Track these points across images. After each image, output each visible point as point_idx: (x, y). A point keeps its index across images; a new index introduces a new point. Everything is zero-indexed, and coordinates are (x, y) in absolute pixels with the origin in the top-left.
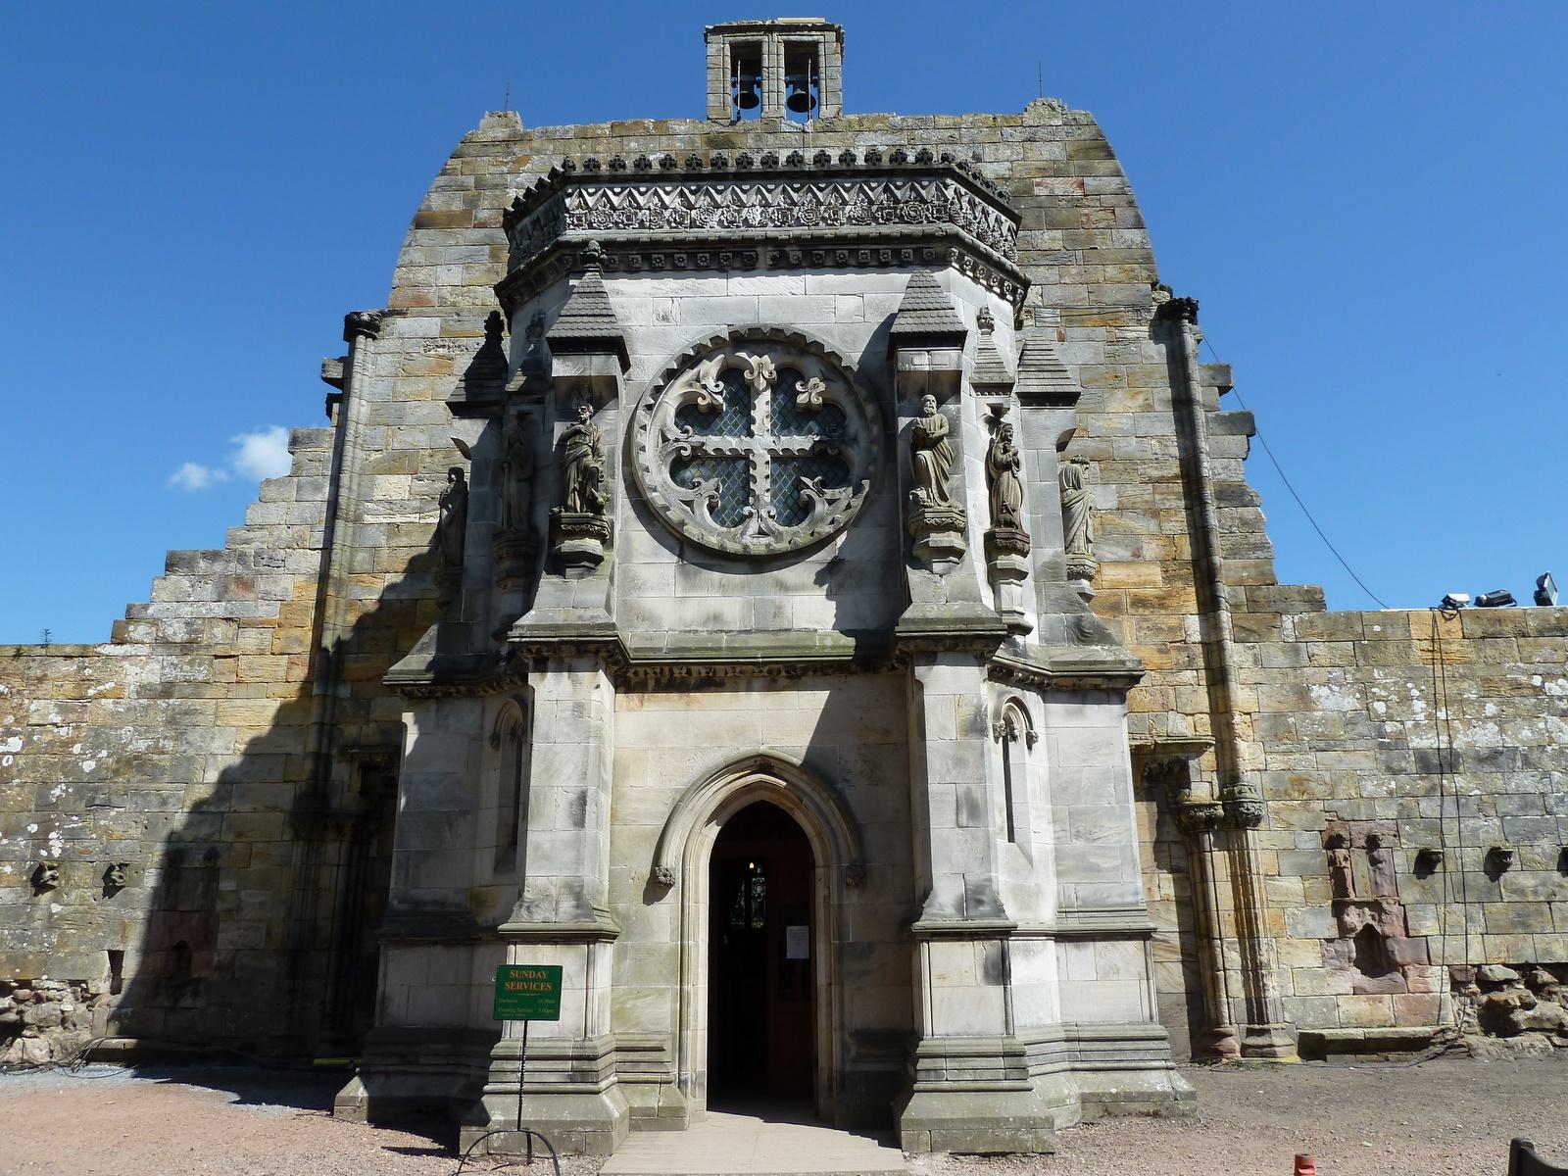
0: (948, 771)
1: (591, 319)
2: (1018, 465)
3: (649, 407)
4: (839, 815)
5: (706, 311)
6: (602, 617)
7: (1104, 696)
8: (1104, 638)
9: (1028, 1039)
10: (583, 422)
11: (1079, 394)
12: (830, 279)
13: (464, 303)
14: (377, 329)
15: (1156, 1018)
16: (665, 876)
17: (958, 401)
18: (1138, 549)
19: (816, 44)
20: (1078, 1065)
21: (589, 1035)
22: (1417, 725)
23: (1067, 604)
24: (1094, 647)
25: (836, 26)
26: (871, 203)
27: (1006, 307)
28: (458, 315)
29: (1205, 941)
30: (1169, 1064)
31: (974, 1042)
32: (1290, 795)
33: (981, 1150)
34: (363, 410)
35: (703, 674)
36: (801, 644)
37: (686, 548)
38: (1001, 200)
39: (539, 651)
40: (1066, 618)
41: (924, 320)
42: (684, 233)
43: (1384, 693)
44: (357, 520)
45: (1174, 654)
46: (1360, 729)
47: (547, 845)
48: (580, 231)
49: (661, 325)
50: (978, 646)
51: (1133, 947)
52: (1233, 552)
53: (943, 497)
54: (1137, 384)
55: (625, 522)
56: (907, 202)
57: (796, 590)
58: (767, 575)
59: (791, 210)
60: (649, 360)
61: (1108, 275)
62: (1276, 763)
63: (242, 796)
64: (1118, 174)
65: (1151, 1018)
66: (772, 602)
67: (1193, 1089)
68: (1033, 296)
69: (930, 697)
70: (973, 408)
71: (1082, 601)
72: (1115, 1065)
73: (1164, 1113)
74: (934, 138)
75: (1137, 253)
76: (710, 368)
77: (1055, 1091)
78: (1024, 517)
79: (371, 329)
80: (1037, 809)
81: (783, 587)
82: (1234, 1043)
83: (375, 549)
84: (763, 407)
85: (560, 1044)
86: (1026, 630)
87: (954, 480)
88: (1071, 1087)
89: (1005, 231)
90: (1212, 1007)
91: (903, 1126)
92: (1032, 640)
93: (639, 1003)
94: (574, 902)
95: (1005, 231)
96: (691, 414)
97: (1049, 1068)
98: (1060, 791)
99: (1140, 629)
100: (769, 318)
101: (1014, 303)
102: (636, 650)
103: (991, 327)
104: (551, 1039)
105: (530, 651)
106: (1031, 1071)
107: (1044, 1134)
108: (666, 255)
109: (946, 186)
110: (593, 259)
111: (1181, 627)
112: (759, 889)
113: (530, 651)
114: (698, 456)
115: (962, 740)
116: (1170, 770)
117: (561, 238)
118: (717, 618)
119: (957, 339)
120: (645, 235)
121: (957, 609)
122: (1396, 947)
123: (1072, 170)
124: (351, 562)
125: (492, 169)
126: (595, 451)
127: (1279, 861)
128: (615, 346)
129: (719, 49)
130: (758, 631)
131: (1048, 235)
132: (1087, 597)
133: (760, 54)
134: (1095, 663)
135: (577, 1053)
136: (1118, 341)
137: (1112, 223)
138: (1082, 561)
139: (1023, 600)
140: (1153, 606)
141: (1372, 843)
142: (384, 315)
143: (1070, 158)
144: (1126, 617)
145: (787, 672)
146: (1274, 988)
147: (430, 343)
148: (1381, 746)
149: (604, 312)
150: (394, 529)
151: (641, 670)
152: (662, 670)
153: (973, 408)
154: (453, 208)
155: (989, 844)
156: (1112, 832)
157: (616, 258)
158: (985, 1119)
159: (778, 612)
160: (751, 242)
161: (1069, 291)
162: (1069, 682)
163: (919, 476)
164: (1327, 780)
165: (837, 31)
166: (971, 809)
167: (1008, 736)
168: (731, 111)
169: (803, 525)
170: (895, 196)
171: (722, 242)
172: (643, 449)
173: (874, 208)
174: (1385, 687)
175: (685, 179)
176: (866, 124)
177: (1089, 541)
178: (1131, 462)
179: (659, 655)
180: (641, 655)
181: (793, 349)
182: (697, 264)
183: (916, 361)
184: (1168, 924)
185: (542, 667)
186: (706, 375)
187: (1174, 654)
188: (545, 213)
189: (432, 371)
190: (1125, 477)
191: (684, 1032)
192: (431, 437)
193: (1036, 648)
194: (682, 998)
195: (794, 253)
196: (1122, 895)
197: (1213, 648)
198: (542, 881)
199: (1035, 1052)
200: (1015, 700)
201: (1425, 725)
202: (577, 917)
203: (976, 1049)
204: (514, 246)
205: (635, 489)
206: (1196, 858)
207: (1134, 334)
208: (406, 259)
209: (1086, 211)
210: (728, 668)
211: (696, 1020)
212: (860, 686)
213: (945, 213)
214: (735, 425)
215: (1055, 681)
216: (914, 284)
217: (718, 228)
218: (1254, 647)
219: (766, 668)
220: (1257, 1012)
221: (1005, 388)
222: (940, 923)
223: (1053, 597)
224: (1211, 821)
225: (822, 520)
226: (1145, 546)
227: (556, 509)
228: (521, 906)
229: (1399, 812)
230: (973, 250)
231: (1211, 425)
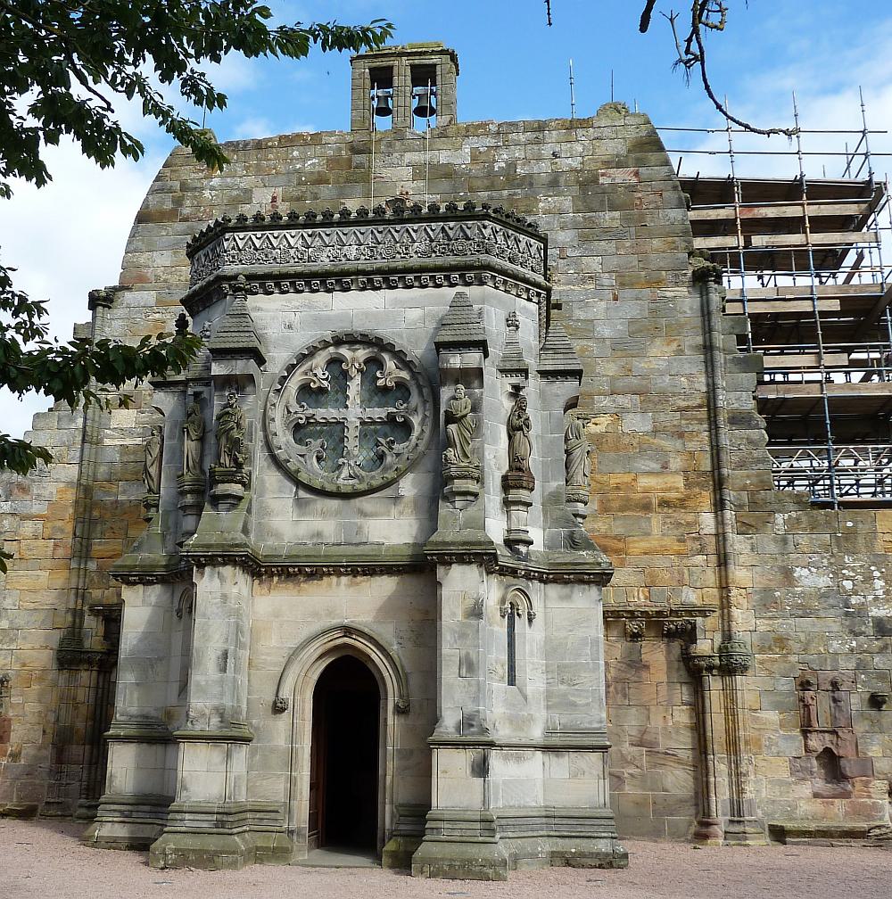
0: (455, 641)
3: (279, 391)
5: (318, 321)
12: (400, 293)
13: (173, 280)
14: (112, 301)
15: (608, 805)
16: (281, 703)
19: (435, 65)
20: (552, 833)
22: (876, 598)
24: (581, 553)
32: (772, 650)
40: (563, 531)
43: (852, 574)
44: (99, 442)
45: (689, 543)
46: (831, 601)
48: (233, 266)
49: (287, 332)
51: (595, 757)
52: (741, 465)
56: (457, 239)
57: (376, 516)
61: (655, 247)
62: (763, 625)
63: (24, 638)
65: (605, 804)
66: (356, 524)
69: (446, 592)
72: (578, 834)
76: (321, 359)
80: (533, 664)
81: (363, 514)
82: (719, 830)
84: (354, 386)
85: (210, 805)
96: (308, 393)
98: (551, 649)
100: (360, 327)
111: (696, 523)
118: (319, 534)
122: (848, 765)
123: (630, 163)
126: (238, 425)
127: (757, 700)
131: (608, 215)
140: (676, 507)
141: (835, 685)
143: (629, 151)
144: (654, 514)
146: (750, 792)
148: (847, 614)
149: (246, 329)
156: (585, 680)
159: (359, 530)
164: (803, 639)
170: (448, 235)
172: (273, 420)
174: (853, 569)
178: (664, 397)
180: (268, 559)
187: (689, 543)
194: (292, 781)
196: (590, 723)
197: (721, 537)
198: (200, 705)
201: (882, 599)
202: (221, 727)
205: (268, 446)
207: (672, 294)
212: (412, 583)
216: (454, 304)
218: (751, 538)
220: (737, 809)
222: (445, 738)
223: (555, 517)
224: (710, 668)
229: (858, 664)
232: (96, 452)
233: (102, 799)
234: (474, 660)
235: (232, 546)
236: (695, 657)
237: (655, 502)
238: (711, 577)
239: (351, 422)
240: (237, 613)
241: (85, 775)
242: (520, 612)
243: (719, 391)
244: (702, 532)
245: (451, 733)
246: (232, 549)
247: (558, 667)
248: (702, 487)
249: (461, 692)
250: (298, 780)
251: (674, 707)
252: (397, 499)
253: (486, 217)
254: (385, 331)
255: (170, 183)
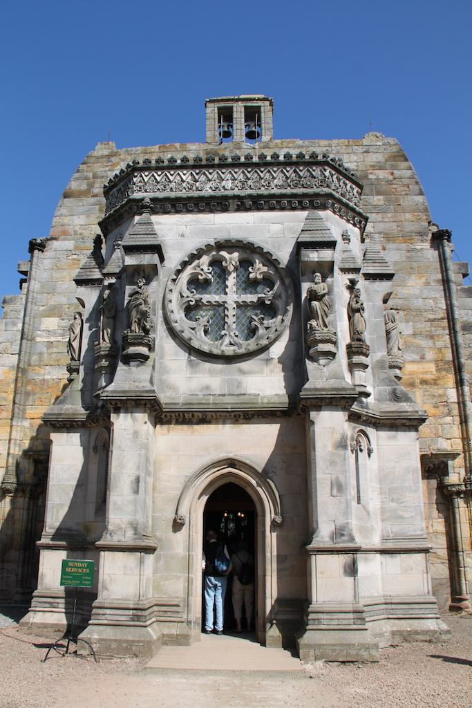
0: (327, 468)
1: (145, 236)
2: (363, 310)
4: (275, 553)
6: (149, 387)
7: (407, 428)
8: (407, 399)
9: (365, 604)
10: (140, 288)
11: (394, 274)
13: (86, 233)
14: (44, 247)
15: (431, 593)
16: (180, 519)
17: (333, 277)
18: (423, 355)
19: (260, 107)
20: (391, 616)
21: (141, 598)
23: (390, 382)
24: (402, 404)
25: (270, 98)
26: (287, 178)
27: (357, 230)
28: (83, 239)
29: (455, 553)
30: (438, 616)
31: (338, 606)
33: (341, 660)
34: (36, 286)
35: (201, 417)
36: (251, 401)
37: (192, 351)
38: (353, 177)
39: (116, 404)
40: (388, 389)
41: (315, 236)
42: (191, 194)
44: (33, 339)
47: (119, 503)
50: (343, 402)
51: (420, 556)
53: (326, 326)
54: (422, 272)
55: (161, 338)
58: (234, 365)
59: (247, 182)
60: (174, 258)
61: (407, 218)
64: (410, 169)
65: (428, 592)
66: (237, 379)
67: (449, 629)
68: (369, 228)
70: (340, 280)
71: (396, 380)
73: (434, 640)
74: (319, 147)
75: (421, 207)
76: (205, 260)
77: (380, 629)
78: (367, 337)
79: (41, 247)
80: (372, 487)
81: (242, 372)
83: (41, 354)
85: (127, 602)
86: (368, 395)
87: (331, 317)
88: (387, 627)
89: (355, 193)
90: (458, 586)
91: (301, 647)
92: (371, 400)
93: (167, 582)
94: (133, 532)
95: (355, 193)
96: (195, 283)
97: (376, 618)
98: (383, 477)
99: (424, 396)
100: (235, 235)
101: (360, 228)
102: (166, 404)
103: (349, 240)
104: (122, 599)
105: (111, 404)
106: (367, 619)
107: (373, 652)
108: (183, 204)
109: (325, 170)
110: (147, 207)
111: (445, 395)
112: (232, 525)
113: (111, 404)
114: (199, 305)
115: (334, 451)
116: (439, 467)
117: (131, 197)
118: (207, 388)
119: (331, 245)
120: (173, 195)
121: (333, 383)
124: (29, 361)
125: (101, 169)
128: (157, 249)
129: (212, 111)
130: (229, 395)
131: (376, 198)
132: (399, 378)
133: (232, 112)
134: (403, 412)
135: (136, 606)
136: (413, 250)
137: (408, 192)
138: (396, 360)
139: (365, 379)
142: (48, 240)
143: (386, 161)
145: (244, 416)
147: (69, 252)
149: (152, 232)
150: (50, 344)
151: (168, 414)
152: (179, 415)
153: (340, 280)
154: (82, 188)
155: (348, 505)
157: (158, 206)
158: (342, 644)
159: (239, 385)
160: (226, 198)
161: (387, 225)
162: (389, 422)
163: (312, 314)
165: (270, 101)
166: (338, 487)
167: (357, 450)
168: (218, 139)
169: (253, 340)
171: (212, 198)
172: (170, 301)
173: (289, 181)
175: (194, 167)
176: (285, 144)
177: (399, 349)
178: (419, 312)
179: (177, 407)
180: (168, 406)
181: (249, 251)
182: (198, 208)
183: (311, 256)
184: (440, 545)
185: (117, 411)
186: (203, 264)
188: (123, 186)
189: (70, 266)
190: (416, 318)
191: (190, 598)
192: (68, 299)
193: (374, 404)
194: (189, 581)
195: (249, 203)
196: (415, 531)
198: (117, 521)
199: (368, 610)
200: (362, 431)
202: (135, 539)
203: (338, 609)
204: (109, 202)
205: (167, 321)
206: (451, 511)
208: (59, 213)
209: (395, 186)
210: (213, 414)
211: (196, 591)
213: (324, 183)
214: (218, 289)
215: (382, 421)
217: (210, 191)
219: (233, 414)
221: (357, 270)
224: (458, 493)
225: (262, 337)
226: (427, 353)
227: (125, 332)
228: (107, 533)
230: (339, 201)
231: (459, 293)
232: (31, 347)
233: (35, 593)
234: (343, 482)
235: (143, 392)
236: (448, 486)
237: (418, 381)
238: (456, 431)
239: (231, 305)
240: (146, 447)
241: (20, 570)
242: (362, 448)
243: (455, 308)
244: (449, 401)
245: (327, 542)
246: (143, 395)
247: (389, 489)
248: (447, 370)
249: (334, 508)
250: (194, 580)
251: (434, 520)
252: (268, 360)
253: (327, 163)
254: (256, 239)
255: (86, 174)
